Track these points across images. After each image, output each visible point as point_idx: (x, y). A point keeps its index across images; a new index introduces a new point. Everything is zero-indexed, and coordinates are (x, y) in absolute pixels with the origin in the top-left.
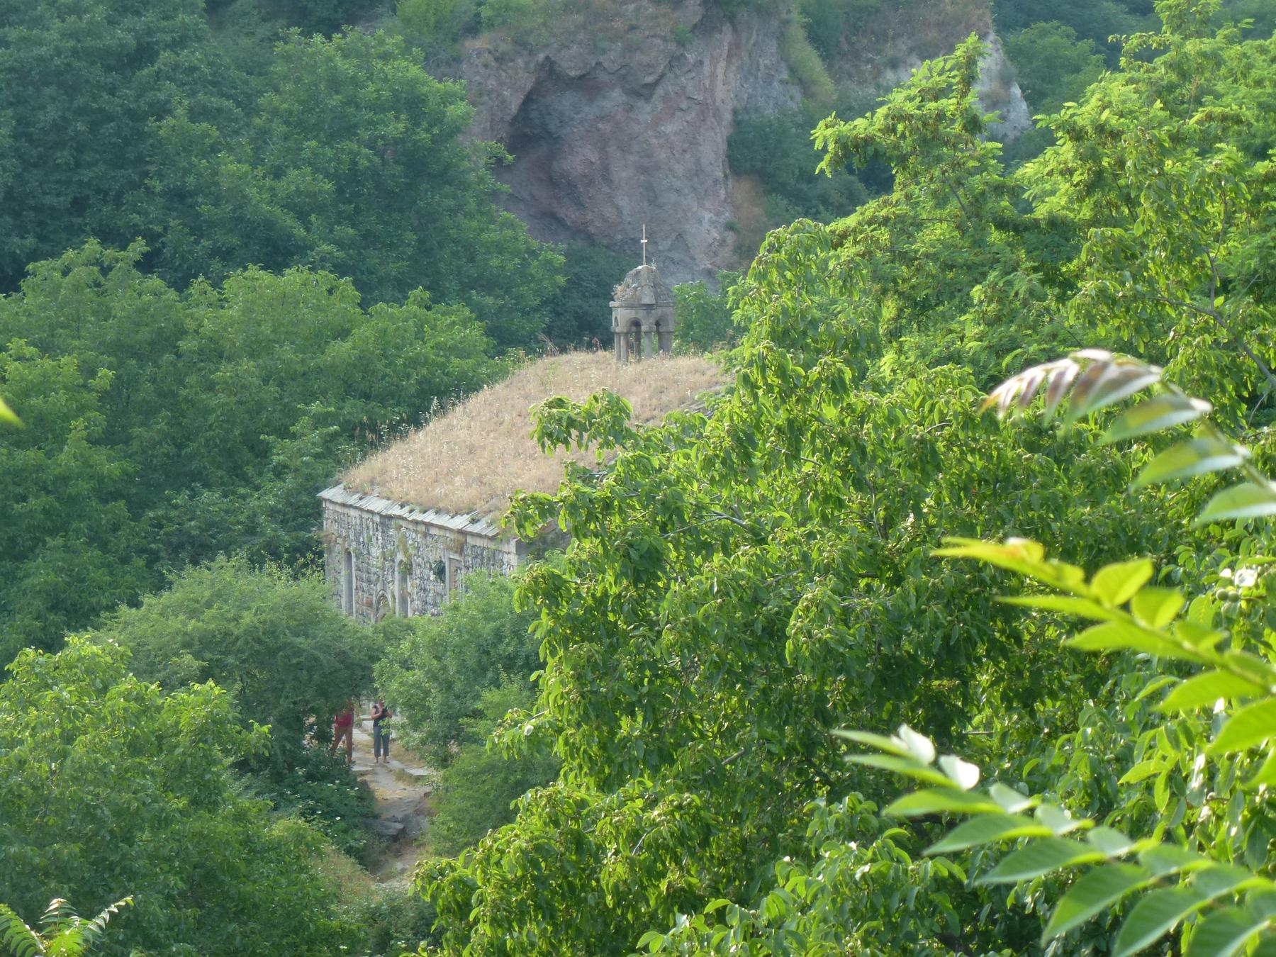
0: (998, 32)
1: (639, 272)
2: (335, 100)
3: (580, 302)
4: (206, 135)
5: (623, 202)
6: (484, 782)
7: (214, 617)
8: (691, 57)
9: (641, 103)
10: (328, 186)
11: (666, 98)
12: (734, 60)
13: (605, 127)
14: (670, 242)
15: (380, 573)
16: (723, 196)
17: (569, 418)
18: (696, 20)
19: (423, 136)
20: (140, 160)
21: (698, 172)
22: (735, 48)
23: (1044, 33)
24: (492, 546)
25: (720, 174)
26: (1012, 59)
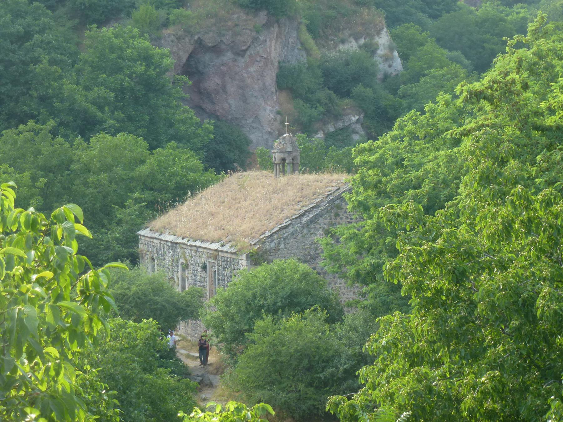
0: (387, 28)
1: (285, 137)
2: (113, 56)
3: (215, 146)
4: (55, 72)
5: (232, 102)
6: (259, 360)
7: (119, 288)
8: (262, 38)
9: (240, 58)
10: (112, 95)
11: (251, 56)
12: (279, 39)
13: (224, 69)
14: (252, 119)
15: (171, 267)
16: (275, 100)
17: (398, 213)
18: (264, 22)
19: (152, 72)
20: (26, 82)
21: (264, 88)
22: (279, 34)
23: (408, 28)
24: (233, 256)
25: (274, 90)
26: (394, 40)
